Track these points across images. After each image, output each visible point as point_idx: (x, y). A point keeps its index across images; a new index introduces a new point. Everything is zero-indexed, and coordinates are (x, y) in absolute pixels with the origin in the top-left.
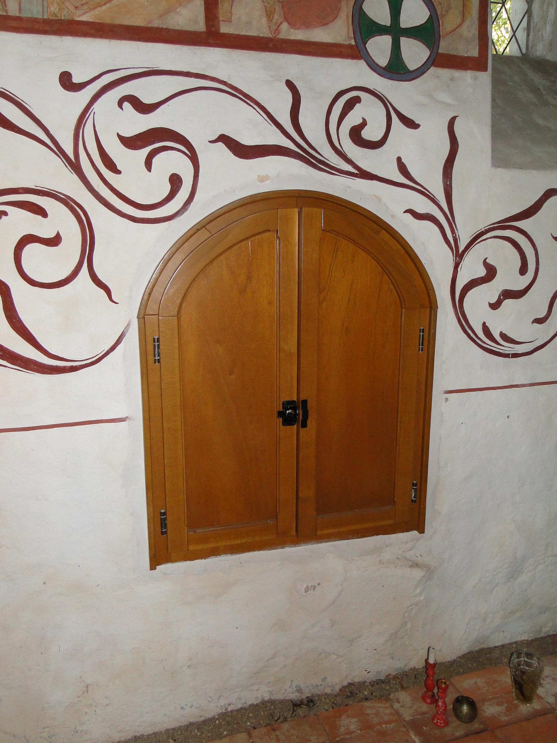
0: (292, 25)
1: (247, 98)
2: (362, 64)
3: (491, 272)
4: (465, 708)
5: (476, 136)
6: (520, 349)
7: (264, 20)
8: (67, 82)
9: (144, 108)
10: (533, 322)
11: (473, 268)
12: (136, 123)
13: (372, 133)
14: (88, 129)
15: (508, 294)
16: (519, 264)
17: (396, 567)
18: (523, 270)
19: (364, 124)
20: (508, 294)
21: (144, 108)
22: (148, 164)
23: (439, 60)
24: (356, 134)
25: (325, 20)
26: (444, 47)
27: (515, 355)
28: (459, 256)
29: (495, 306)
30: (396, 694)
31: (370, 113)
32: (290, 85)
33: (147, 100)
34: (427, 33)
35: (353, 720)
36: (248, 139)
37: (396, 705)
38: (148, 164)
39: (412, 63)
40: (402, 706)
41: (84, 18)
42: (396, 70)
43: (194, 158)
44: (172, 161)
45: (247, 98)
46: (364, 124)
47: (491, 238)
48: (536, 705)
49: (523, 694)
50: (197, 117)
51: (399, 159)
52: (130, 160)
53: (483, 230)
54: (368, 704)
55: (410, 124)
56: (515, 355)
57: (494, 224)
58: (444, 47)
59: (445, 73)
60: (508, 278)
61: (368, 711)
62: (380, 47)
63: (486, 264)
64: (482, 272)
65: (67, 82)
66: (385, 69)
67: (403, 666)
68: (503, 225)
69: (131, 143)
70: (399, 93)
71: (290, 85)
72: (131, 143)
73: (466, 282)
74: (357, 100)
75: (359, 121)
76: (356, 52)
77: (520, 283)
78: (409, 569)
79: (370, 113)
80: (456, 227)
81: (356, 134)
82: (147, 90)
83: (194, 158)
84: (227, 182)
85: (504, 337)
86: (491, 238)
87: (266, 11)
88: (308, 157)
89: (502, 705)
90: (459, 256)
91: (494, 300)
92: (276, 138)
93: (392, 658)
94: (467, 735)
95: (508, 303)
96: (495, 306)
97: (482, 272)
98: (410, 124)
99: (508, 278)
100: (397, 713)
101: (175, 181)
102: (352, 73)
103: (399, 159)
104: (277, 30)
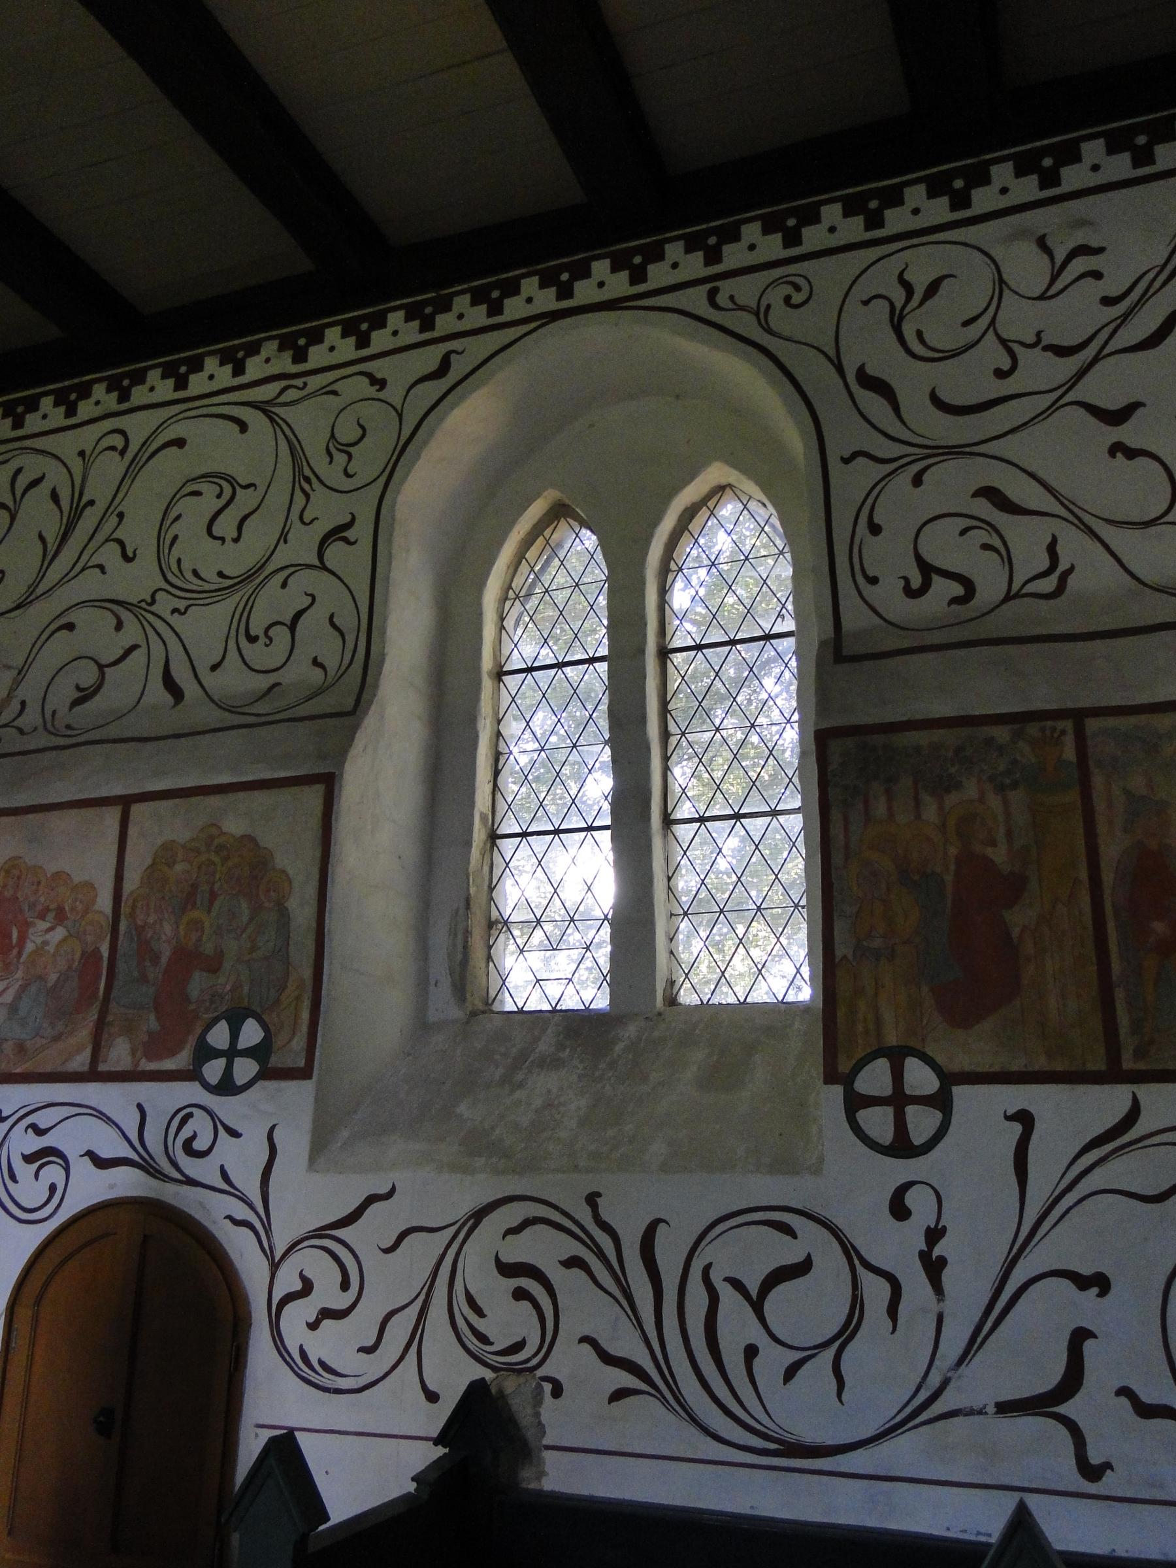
0: (150, 1059)
1: (109, 1120)
2: (196, 1085)
3: (307, 1287)
5: (294, 1143)
6: (342, 1383)
7: (129, 1058)
8: (101, 568)
9: (40, 1132)
11: (288, 1281)
12: (35, 1144)
13: (200, 1145)
14: (293, 569)
15: (327, 1313)
16: (340, 1279)
18: (345, 1285)
19: (194, 1137)
20: (327, 1313)
21: (40, 1132)
22: (37, 1176)
23: (267, 1073)
24: (188, 1147)
25: (172, 1053)
26: (275, 1061)
28: (275, 1267)
29: (313, 1326)
31: (200, 1125)
32: (140, 1107)
33: (42, 1126)
34: (259, 1052)
36: (105, 1154)
38: (37, 1176)
39: (240, 1080)
41: (18, 1071)
42: (226, 1087)
43: (67, 1170)
44: (53, 1173)
45: (109, 1120)
46: (194, 1137)
50: (74, 1137)
51: (222, 1167)
52: (25, 1171)
55: (234, 1134)
58: (275, 1061)
59: (271, 1085)
60: (328, 1294)
62: (213, 1070)
63: (302, 1277)
64: (298, 1286)
65: (101, 568)
66: (215, 1087)
68: (319, 1233)
69: (28, 1159)
70: (228, 1108)
71: (140, 1107)
72: (28, 1159)
74: (190, 1115)
75: (191, 1134)
76: (193, 1074)
77: (341, 1301)
79: (200, 1125)
80: (976, 1351)
81: (188, 1147)
82: (43, 1119)
83: (67, 1170)
84: (89, 1188)
85: (322, 1363)
88: (148, 1167)
90: (275, 1267)
91: (312, 1320)
92: (125, 1152)
95: (326, 1323)
96: (313, 1326)
97: (298, 1286)
98: (234, 1134)
99: (328, 1294)
101: (53, 1188)
102: (189, 1092)
103: (222, 1167)
104: (137, 1065)
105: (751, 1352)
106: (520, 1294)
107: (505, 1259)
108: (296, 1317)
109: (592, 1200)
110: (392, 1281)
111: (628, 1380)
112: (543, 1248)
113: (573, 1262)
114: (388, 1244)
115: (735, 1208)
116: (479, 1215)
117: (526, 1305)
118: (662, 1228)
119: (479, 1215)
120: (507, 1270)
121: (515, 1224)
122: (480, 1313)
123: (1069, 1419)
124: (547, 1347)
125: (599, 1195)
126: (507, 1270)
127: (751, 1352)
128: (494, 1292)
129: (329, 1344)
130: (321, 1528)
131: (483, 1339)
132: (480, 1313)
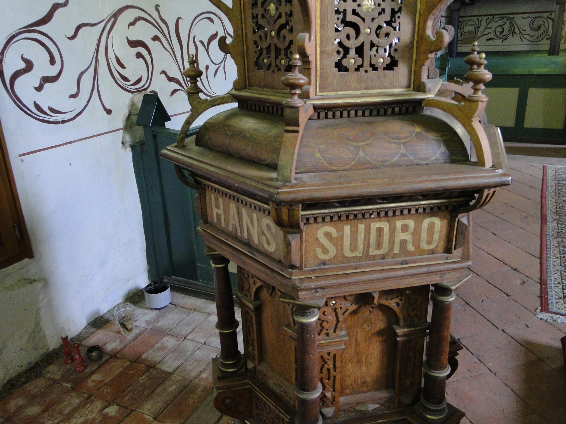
4: (94, 354)
10: (69, 97)
17: (19, 288)
18: (52, 62)
20: (46, 80)
27: (63, 122)
29: (39, 89)
30: (46, 369)
35: (19, 399)
37: (48, 375)
40: (53, 373)
47: (203, 19)
48: (136, 331)
49: (127, 329)
53: (14, 33)
54: (27, 385)
56: (63, 122)
57: (21, 29)
60: (43, 68)
61: (29, 388)
67: (45, 351)
68: (29, 29)
73: (9, 77)
77: (52, 71)
78: (30, 285)
85: (51, 110)
86: (203, 19)
87: (202, 177)
89: (116, 341)
91: (37, 85)
93: (36, 350)
94: (100, 367)
95: (47, 86)
96: (39, 89)
99: (43, 68)
100: (50, 379)
105: (207, 67)
106: (139, 55)
107: (132, 39)
108: (25, 86)
109: (157, 7)
110: (77, 55)
111: (178, 87)
112: (143, 32)
113: (156, 38)
114: (71, 34)
115: (49, 35)
116: (116, 15)
117: (141, 59)
118: (180, 20)
119: (116, 15)
120: (134, 44)
121: (132, 21)
122: (123, 66)
123: (54, 58)
124: (150, 78)
125: (159, 6)
126: (134, 44)
127: (207, 67)
128: (128, 54)
129: (50, 97)
130: (235, 369)
131: (125, 79)
132: (123, 66)
